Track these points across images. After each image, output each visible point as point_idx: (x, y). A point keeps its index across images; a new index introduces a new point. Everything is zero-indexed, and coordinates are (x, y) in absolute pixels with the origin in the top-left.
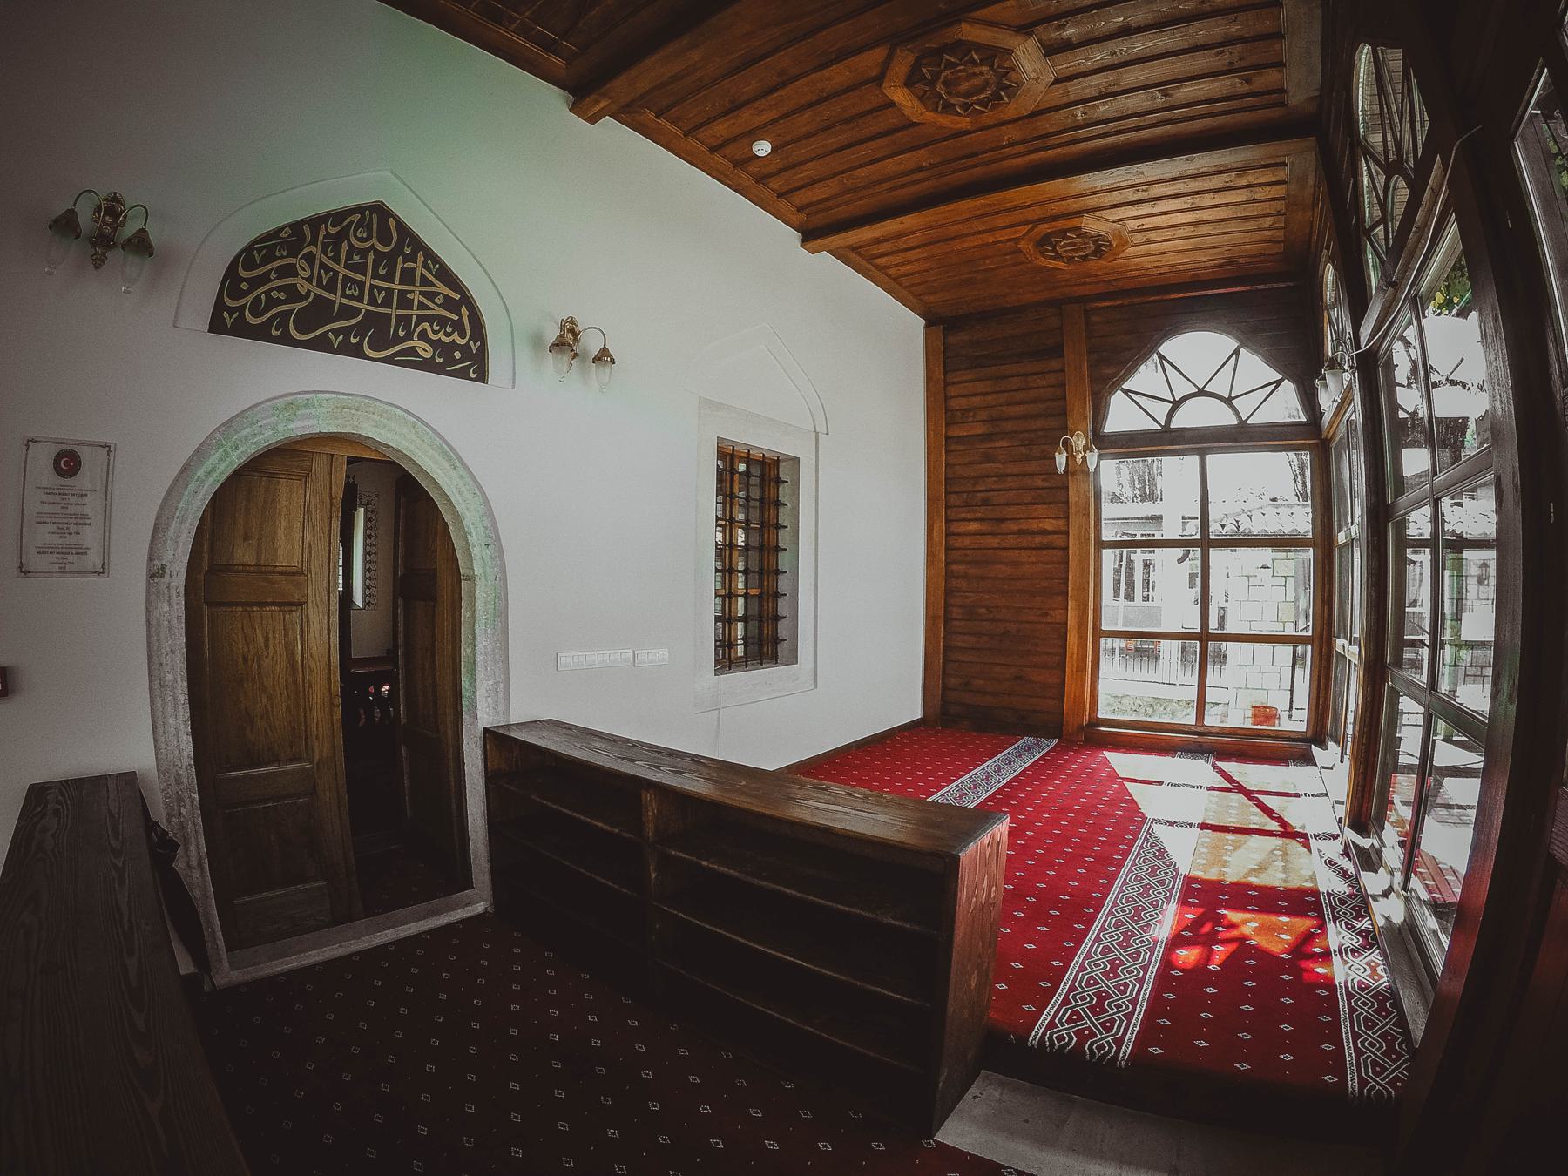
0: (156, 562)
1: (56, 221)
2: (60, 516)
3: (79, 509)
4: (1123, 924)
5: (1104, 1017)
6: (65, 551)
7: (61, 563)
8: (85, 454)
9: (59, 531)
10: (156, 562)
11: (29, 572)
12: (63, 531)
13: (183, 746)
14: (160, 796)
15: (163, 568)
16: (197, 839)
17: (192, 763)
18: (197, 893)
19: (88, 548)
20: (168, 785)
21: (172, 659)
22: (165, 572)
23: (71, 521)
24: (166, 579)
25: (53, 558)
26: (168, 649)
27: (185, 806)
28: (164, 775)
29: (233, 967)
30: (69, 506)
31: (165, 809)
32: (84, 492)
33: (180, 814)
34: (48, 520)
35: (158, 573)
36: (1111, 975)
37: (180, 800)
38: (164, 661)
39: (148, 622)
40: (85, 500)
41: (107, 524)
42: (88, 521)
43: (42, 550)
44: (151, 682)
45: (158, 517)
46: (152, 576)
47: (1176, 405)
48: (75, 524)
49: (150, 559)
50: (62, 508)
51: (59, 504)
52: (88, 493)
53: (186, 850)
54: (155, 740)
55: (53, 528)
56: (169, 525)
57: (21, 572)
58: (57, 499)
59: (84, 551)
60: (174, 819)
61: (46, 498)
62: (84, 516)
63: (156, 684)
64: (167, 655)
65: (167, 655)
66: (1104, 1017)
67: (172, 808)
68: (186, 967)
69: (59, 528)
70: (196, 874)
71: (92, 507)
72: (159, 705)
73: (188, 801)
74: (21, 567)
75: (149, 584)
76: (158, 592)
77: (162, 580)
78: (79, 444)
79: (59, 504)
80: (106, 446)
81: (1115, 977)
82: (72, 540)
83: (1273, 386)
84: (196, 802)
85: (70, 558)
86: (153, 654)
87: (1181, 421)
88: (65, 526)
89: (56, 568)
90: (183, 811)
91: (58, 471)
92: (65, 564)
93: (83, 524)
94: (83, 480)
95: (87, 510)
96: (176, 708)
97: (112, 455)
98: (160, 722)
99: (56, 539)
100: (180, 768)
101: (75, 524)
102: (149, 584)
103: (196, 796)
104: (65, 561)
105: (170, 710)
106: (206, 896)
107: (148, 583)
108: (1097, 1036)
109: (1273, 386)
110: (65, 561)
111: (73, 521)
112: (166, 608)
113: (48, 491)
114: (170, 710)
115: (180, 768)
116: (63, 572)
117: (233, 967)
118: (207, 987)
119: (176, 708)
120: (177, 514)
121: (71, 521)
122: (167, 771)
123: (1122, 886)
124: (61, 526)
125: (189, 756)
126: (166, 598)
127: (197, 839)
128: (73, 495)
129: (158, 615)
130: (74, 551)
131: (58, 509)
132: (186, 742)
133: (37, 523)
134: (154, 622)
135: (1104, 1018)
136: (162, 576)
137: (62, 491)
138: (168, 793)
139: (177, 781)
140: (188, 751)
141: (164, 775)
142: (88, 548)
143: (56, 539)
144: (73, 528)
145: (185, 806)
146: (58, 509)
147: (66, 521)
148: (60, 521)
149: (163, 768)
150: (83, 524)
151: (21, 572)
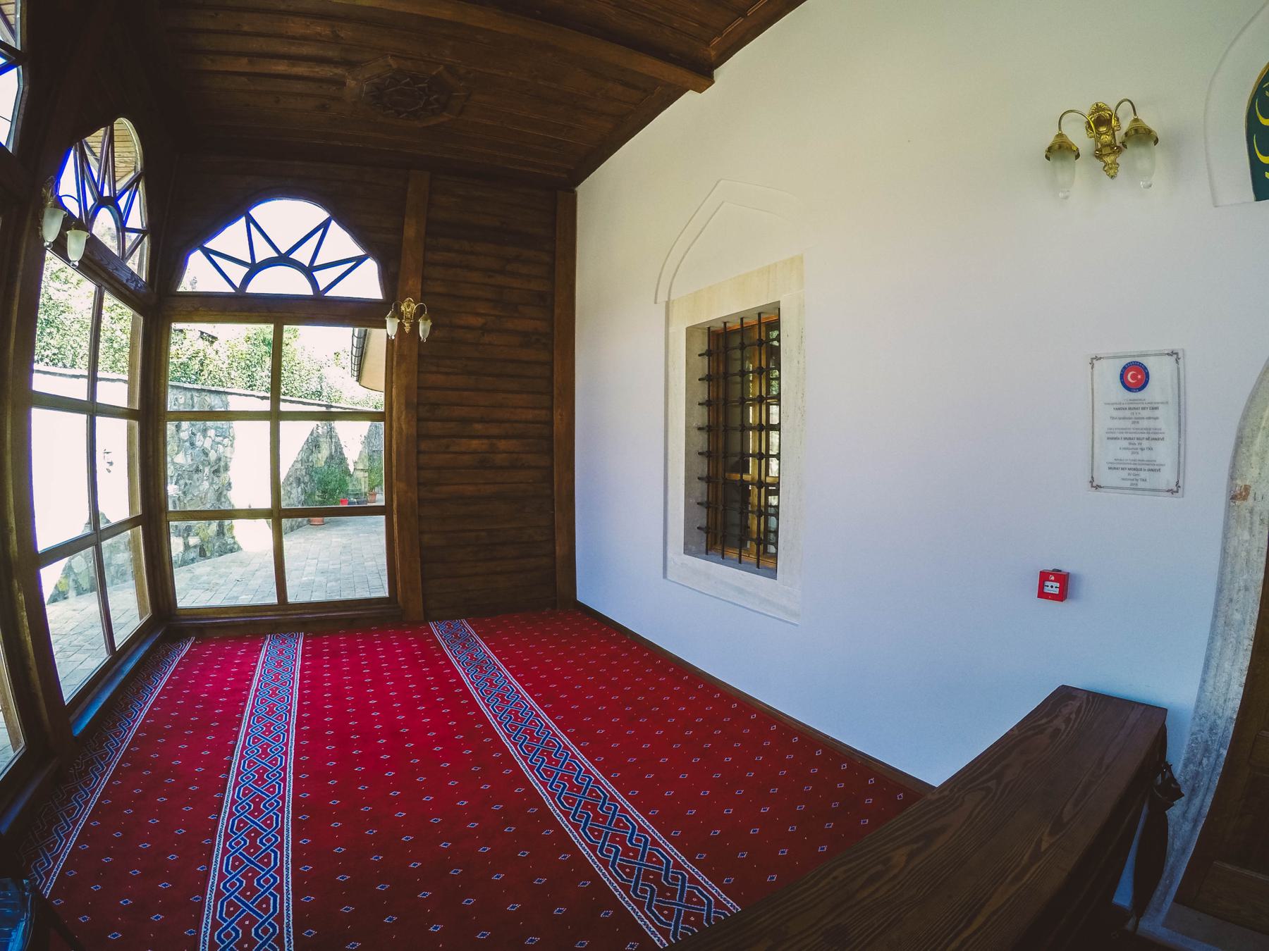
0: (1239, 482)
1: (1050, 149)
2: (1132, 431)
3: (1151, 424)
4: (266, 701)
5: (246, 830)
6: (1139, 467)
7: (1133, 480)
8: (1149, 363)
9: (1131, 446)
10: (1239, 482)
11: (1100, 487)
12: (1135, 447)
13: (1231, 695)
14: (1187, 740)
15: (1247, 488)
16: (1205, 796)
17: (1235, 717)
18: (1178, 844)
19: (1162, 465)
20: (1200, 730)
21: (1245, 596)
22: (1248, 494)
23: (1143, 436)
24: (1250, 501)
25: (1124, 474)
26: (1242, 584)
27: (1209, 757)
28: (1200, 719)
29: (1164, 925)
30: (1140, 421)
31: (1188, 753)
32: (1156, 406)
33: (1201, 763)
34: (1119, 436)
35: (1241, 494)
36: (257, 800)
37: (1207, 750)
38: (1235, 597)
39: (1224, 550)
40: (1157, 413)
41: (1182, 437)
42: (1161, 436)
43: (1113, 466)
44: (1215, 616)
45: (1241, 430)
46: (1234, 498)
47: (255, 268)
48: (1147, 439)
49: (1232, 478)
50: (1134, 423)
51: (1130, 418)
52: (1160, 406)
53: (1190, 800)
54: (1204, 681)
55: (1125, 443)
56: (1254, 437)
57: (1092, 486)
58: (1128, 413)
59: (1157, 468)
60: (1191, 765)
61: (1116, 413)
62: (1156, 431)
63: (1221, 621)
64: (1239, 590)
65: (1239, 590)
66: (246, 830)
67: (1194, 755)
68: (1123, 897)
69: (1130, 444)
70: (1187, 827)
71: (1165, 420)
72: (1218, 644)
73: (1214, 755)
74: (1092, 482)
75: (1230, 506)
76: (1239, 516)
77: (1245, 503)
78: (1145, 355)
79: (1130, 418)
80: (1172, 353)
81: (273, 713)
82: (1145, 455)
83: (252, 226)
84: (1222, 760)
85: (1143, 475)
86: (1225, 586)
87: (254, 287)
88: (1136, 442)
89: (1127, 484)
90: (1205, 761)
91: (1127, 386)
92: (1137, 480)
93: (1156, 439)
94: (1153, 391)
95: (1161, 424)
96: (1236, 652)
97: (1181, 361)
98: (1214, 663)
99: (1127, 455)
100: (1220, 718)
101: (1148, 439)
102: (1230, 506)
103: (1225, 753)
104: (1137, 477)
105: (1229, 652)
106: (1184, 850)
107: (1229, 509)
108: (274, 872)
109: (252, 226)
110: (1137, 477)
111: (1146, 436)
112: (1246, 536)
113: (1118, 406)
114: (1229, 652)
115: (1220, 718)
116: (1134, 489)
117: (1164, 925)
118: (1129, 926)
119: (1236, 652)
120: (1263, 425)
121: (1143, 436)
122: (1205, 716)
123: (247, 730)
124: (1132, 441)
125: (1233, 709)
126: (1248, 524)
127: (1205, 796)
128: (1143, 409)
129: (1236, 544)
130: (1147, 467)
131: (1128, 424)
132: (1237, 691)
133: (1108, 439)
134: (1231, 551)
135: (263, 817)
136: (1245, 498)
137: (1132, 406)
138: (1197, 739)
139: (1211, 730)
140: (1237, 703)
141: (1200, 719)
142: (1162, 465)
143: (1127, 455)
144: (1145, 444)
145: (1209, 757)
146: (1128, 424)
147: (1138, 436)
148: (1134, 436)
149: (1201, 712)
150: (1156, 439)
151: (1092, 486)
